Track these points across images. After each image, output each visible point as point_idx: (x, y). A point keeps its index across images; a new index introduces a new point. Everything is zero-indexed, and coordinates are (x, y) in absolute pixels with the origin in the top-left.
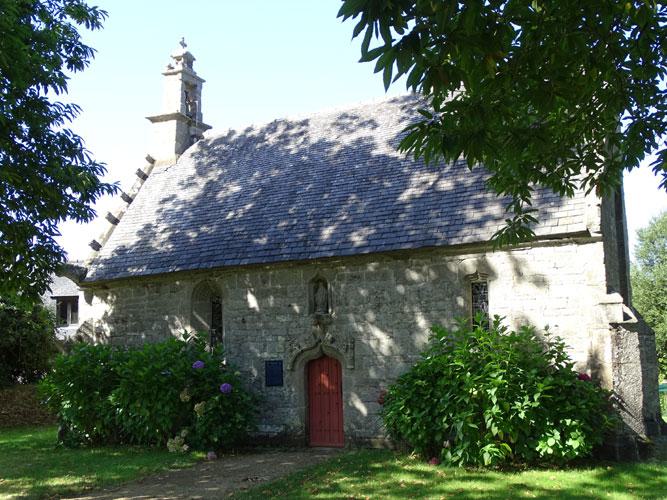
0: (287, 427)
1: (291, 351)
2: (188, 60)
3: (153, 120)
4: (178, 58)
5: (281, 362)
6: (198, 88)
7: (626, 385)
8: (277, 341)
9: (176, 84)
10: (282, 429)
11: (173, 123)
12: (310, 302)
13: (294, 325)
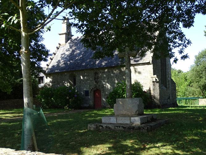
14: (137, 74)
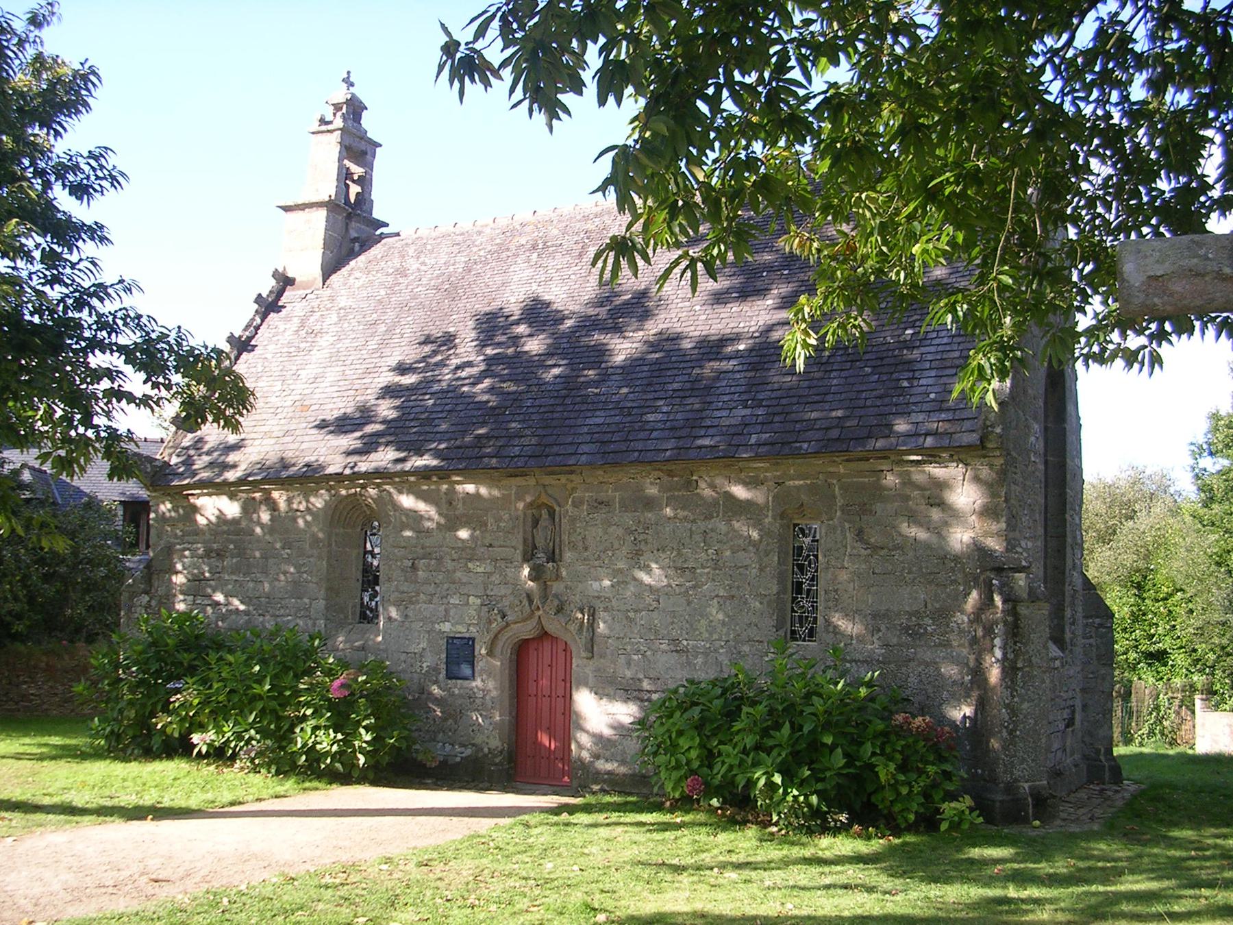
0: (479, 748)
1: (490, 622)
2: (354, 109)
3: (287, 209)
4: (337, 107)
5: (473, 640)
6: (369, 157)
7: (1023, 700)
8: (467, 604)
9: (330, 146)
10: (469, 752)
11: (322, 214)
12: (525, 540)
13: (496, 578)
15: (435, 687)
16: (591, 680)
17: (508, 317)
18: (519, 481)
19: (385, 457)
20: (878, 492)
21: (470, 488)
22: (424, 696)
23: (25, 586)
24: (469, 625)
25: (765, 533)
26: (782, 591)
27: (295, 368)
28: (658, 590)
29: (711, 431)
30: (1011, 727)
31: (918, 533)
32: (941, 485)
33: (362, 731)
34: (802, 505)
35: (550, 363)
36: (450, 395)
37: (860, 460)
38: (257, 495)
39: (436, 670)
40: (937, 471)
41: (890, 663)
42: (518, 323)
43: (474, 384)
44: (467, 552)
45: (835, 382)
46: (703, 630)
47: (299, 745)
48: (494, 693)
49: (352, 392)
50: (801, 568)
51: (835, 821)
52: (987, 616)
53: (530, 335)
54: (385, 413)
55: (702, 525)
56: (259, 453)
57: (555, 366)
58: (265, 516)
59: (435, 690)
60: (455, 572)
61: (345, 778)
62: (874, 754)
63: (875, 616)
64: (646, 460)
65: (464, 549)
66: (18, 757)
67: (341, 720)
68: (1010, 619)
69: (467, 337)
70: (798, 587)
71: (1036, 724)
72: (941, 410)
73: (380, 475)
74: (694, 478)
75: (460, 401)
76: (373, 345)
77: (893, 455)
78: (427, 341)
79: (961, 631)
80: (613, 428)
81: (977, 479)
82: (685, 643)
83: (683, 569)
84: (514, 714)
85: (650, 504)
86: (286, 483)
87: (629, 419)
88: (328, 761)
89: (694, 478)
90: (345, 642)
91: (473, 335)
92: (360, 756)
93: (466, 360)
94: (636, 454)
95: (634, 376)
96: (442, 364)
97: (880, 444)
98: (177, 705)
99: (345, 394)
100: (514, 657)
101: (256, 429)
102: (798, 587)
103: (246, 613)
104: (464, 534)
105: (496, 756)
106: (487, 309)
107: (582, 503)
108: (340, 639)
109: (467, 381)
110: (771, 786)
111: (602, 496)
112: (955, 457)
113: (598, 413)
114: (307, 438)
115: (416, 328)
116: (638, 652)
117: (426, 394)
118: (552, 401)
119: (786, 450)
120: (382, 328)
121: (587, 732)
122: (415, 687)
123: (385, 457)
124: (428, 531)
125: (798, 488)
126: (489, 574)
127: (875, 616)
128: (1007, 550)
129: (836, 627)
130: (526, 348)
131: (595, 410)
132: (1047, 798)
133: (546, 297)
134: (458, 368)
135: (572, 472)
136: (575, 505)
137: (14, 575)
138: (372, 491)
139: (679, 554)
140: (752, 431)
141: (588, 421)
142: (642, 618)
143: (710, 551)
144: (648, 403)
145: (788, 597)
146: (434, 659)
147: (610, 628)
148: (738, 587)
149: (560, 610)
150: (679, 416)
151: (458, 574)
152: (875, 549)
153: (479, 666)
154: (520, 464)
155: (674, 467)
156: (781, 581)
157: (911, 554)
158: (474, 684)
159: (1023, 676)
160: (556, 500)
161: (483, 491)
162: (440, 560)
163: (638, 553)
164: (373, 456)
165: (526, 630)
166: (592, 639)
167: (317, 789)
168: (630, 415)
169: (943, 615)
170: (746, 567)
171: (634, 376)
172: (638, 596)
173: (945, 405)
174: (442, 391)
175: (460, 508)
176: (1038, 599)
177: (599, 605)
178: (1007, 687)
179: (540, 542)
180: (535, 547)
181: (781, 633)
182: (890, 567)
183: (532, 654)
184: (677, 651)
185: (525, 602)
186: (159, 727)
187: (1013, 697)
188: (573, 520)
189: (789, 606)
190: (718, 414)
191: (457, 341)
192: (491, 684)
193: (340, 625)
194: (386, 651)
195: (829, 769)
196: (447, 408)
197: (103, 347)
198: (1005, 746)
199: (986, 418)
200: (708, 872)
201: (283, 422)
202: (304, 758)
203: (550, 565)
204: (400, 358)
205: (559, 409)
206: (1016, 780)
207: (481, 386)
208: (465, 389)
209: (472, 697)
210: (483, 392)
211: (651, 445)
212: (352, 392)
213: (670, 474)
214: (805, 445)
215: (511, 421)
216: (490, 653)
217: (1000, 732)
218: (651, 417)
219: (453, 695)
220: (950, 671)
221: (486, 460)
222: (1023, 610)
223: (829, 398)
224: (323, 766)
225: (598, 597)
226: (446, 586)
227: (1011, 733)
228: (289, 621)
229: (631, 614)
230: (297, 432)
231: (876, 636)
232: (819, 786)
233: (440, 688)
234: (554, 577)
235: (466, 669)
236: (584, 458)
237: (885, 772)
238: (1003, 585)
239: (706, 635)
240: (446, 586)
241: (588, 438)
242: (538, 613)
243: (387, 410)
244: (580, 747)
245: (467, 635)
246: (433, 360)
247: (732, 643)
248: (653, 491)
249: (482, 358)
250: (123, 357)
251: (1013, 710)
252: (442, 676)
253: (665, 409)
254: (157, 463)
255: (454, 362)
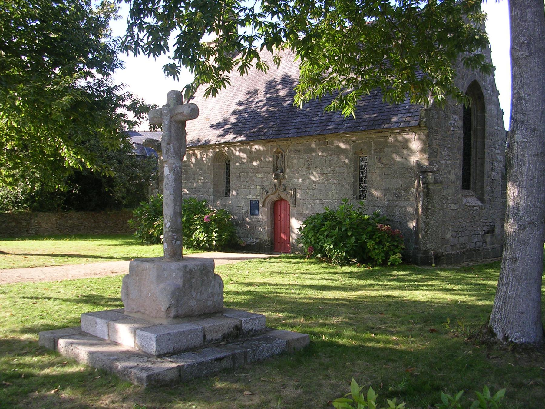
1: (263, 195)
5: (258, 201)
10: (258, 241)
12: (274, 165)
13: (265, 179)
14: (238, 73)
15: (247, 218)
16: (295, 214)
17: (276, 82)
18: (271, 144)
19: (230, 137)
20: (386, 143)
21: (257, 147)
22: (244, 222)
23: (124, 187)
24: (257, 196)
25: (350, 161)
26: (356, 181)
27: (206, 105)
28: (315, 182)
29: (333, 123)
30: (426, 230)
31: (398, 158)
32: (407, 141)
33: (214, 233)
34: (361, 149)
35: (287, 99)
36: (253, 113)
37: (379, 132)
38: (191, 152)
39: (247, 212)
40: (407, 136)
41: (390, 207)
42: (279, 84)
43: (262, 108)
44: (256, 170)
45: (376, 103)
46: (330, 196)
47: (194, 238)
48: (266, 220)
49: (223, 113)
50: (362, 172)
51: (352, 261)
52: (419, 189)
53: (282, 89)
54: (232, 120)
55: (329, 158)
56: (191, 137)
57: (288, 100)
58: (193, 160)
59: (248, 220)
60: (252, 177)
61: (209, 250)
62: (366, 239)
63: (385, 190)
64: (310, 135)
65: (255, 169)
66: (116, 245)
67: (207, 229)
68: (425, 190)
69: (262, 89)
70: (361, 180)
71: (436, 229)
72: (408, 113)
73: (227, 144)
74: (327, 141)
75: (256, 115)
76: (232, 95)
77: (390, 130)
78: (249, 93)
79: (413, 195)
80: (302, 123)
81: (419, 139)
82: (324, 201)
83: (323, 174)
84: (273, 227)
85: (312, 150)
86: (198, 148)
87: (308, 119)
88: (203, 243)
89: (327, 141)
90: (220, 203)
91: (264, 90)
92: (214, 242)
93: (260, 99)
94: (308, 133)
95: (312, 103)
96: (252, 101)
97: (386, 126)
98: (156, 226)
99: (221, 114)
100: (272, 207)
101: (192, 128)
102: (361, 180)
103: (188, 194)
104: (255, 164)
105: (266, 242)
106: (270, 79)
107: (291, 151)
108: (218, 202)
109: (259, 107)
110: (330, 248)
111: (297, 148)
112: (411, 130)
113: (299, 118)
114: (207, 131)
115: (246, 87)
116: (310, 204)
117: (245, 113)
118: (285, 114)
119: (355, 130)
120: (236, 88)
121: (294, 233)
122: (241, 219)
123: (230, 137)
124: (244, 163)
125: (360, 143)
126: (263, 178)
127: (385, 190)
128: (429, 164)
129: (372, 194)
130: (280, 94)
131: (298, 117)
132: (441, 256)
133: (290, 74)
134: (258, 102)
135: (287, 140)
136: (289, 152)
137: (120, 184)
138: (226, 149)
139: (322, 169)
140: (346, 122)
141: (295, 121)
142: (311, 192)
143: (332, 167)
144: (315, 113)
145: (358, 183)
146: (247, 209)
147: (301, 196)
148: (341, 180)
149: (285, 190)
150: (324, 118)
151: (253, 178)
152: (385, 165)
153: (261, 210)
154: (271, 138)
155: (319, 137)
156: (355, 177)
157: (396, 167)
158: (259, 217)
159: (431, 211)
160: (283, 150)
161: (261, 148)
162: (247, 173)
163: (309, 169)
164: (226, 137)
165: (275, 197)
166: (295, 200)
167: (198, 253)
168: (308, 118)
169: (407, 189)
170: (343, 173)
171: (312, 103)
172: (310, 184)
173: (411, 111)
174: (251, 112)
175: (253, 155)
176: (437, 183)
177: (297, 188)
178: (424, 215)
179: (279, 166)
180: (277, 167)
181: (355, 196)
182: (390, 172)
183: (279, 206)
184: (322, 204)
185: (274, 187)
186: (150, 233)
187: (427, 219)
188: (288, 158)
189: (358, 186)
190: (336, 117)
191: (259, 92)
192: (264, 217)
193: (219, 198)
194: (232, 206)
195: (349, 244)
196: (252, 118)
197: (121, 106)
198: (423, 237)
199: (421, 116)
200: (291, 275)
201: (201, 125)
202: (195, 242)
203: (281, 174)
204: (240, 99)
205: (287, 116)
206: (428, 250)
207: (263, 109)
208: (259, 110)
209: (259, 222)
210: (264, 112)
211: (313, 129)
212: (223, 113)
213: (319, 140)
214: (361, 128)
215: (271, 122)
216: (263, 206)
217: (422, 232)
218: (315, 119)
219: (253, 221)
220: (410, 209)
221: (260, 137)
222: (431, 187)
223: (373, 109)
224: (201, 245)
225: (297, 185)
226: (250, 182)
227: (426, 232)
228: (202, 197)
229: (307, 191)
230: (204, 129)
231: (385, 197)
232: (345, 249)
233: (249, 218)
234: (283, 178)
235: (257, 212)
236: (291, 135)
237: (370, 244)
238: (424, 178)
239: (331, 198)
240: (250, 182)
241: (293, 127)
242: (278, 191)
243: (233, 120)
244: (293, 238)
245: (256, 200)
246: (250, 100)
247: (339, 200)
248: (313, 146)
249: (265, 98)
250: (127, 109)
251: (426, 224)
252: (249, 214)
253: (320, 115)
254: (159, 142)
255: (257, 100)
